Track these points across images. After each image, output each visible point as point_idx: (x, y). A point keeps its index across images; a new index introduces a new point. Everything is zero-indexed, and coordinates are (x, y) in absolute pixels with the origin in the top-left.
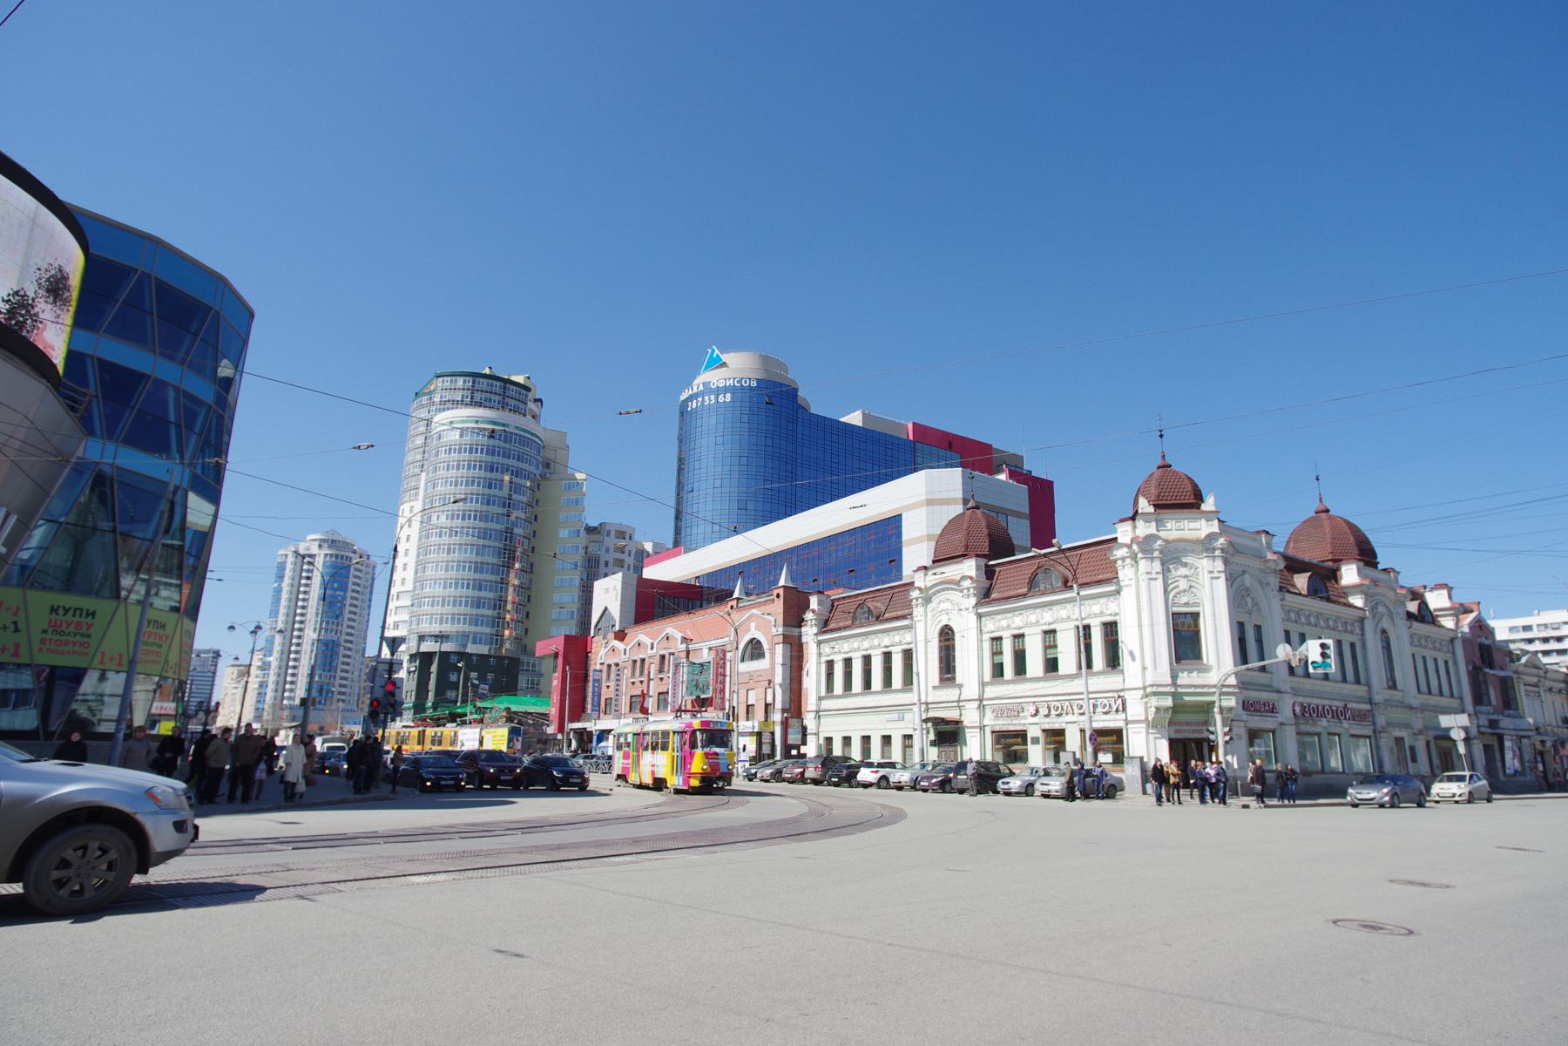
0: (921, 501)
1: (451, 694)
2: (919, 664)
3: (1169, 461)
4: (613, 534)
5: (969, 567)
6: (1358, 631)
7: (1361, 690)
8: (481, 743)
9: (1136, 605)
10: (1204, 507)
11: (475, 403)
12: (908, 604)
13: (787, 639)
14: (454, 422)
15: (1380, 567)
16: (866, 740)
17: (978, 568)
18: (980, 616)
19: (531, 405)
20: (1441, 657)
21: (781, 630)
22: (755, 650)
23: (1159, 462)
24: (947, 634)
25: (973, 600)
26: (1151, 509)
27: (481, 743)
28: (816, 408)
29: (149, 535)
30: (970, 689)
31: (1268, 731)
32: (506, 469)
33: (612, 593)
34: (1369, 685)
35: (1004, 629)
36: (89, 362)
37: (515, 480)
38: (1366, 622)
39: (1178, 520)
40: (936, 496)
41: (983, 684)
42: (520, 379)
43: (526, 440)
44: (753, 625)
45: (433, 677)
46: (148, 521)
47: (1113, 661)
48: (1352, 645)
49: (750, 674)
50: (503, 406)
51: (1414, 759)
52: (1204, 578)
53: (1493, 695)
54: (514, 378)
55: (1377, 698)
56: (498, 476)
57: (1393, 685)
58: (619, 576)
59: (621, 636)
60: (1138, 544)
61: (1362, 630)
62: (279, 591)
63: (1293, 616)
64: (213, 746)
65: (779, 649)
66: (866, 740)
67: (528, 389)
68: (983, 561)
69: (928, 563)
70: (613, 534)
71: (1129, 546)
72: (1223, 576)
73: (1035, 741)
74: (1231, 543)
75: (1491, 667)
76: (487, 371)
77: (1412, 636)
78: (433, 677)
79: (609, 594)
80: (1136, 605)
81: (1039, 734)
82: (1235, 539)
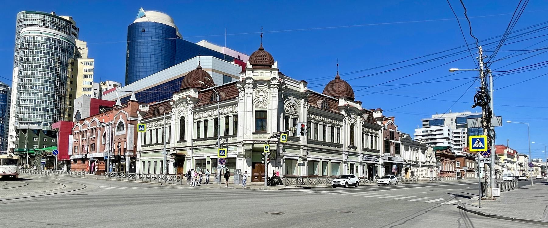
3: (263, 47)
8: (187, 158)
9: (245, 108)
10: (273, 67)
15: (355, 100)
23: (260, 47)
24: (183, 120)
26: (251, 67)
27: (187, 158)
28: (185, 38)
30: (189, 142)
35: (201, 118)
39: (260, 71)
42: (67, 18)
49: (120, 136)
51: (357, 171)
52: (270, 96)
53: (392, 149)
64: (259, 154)
72: (277, 96)
75: (393, 140)
76: (52, 13)
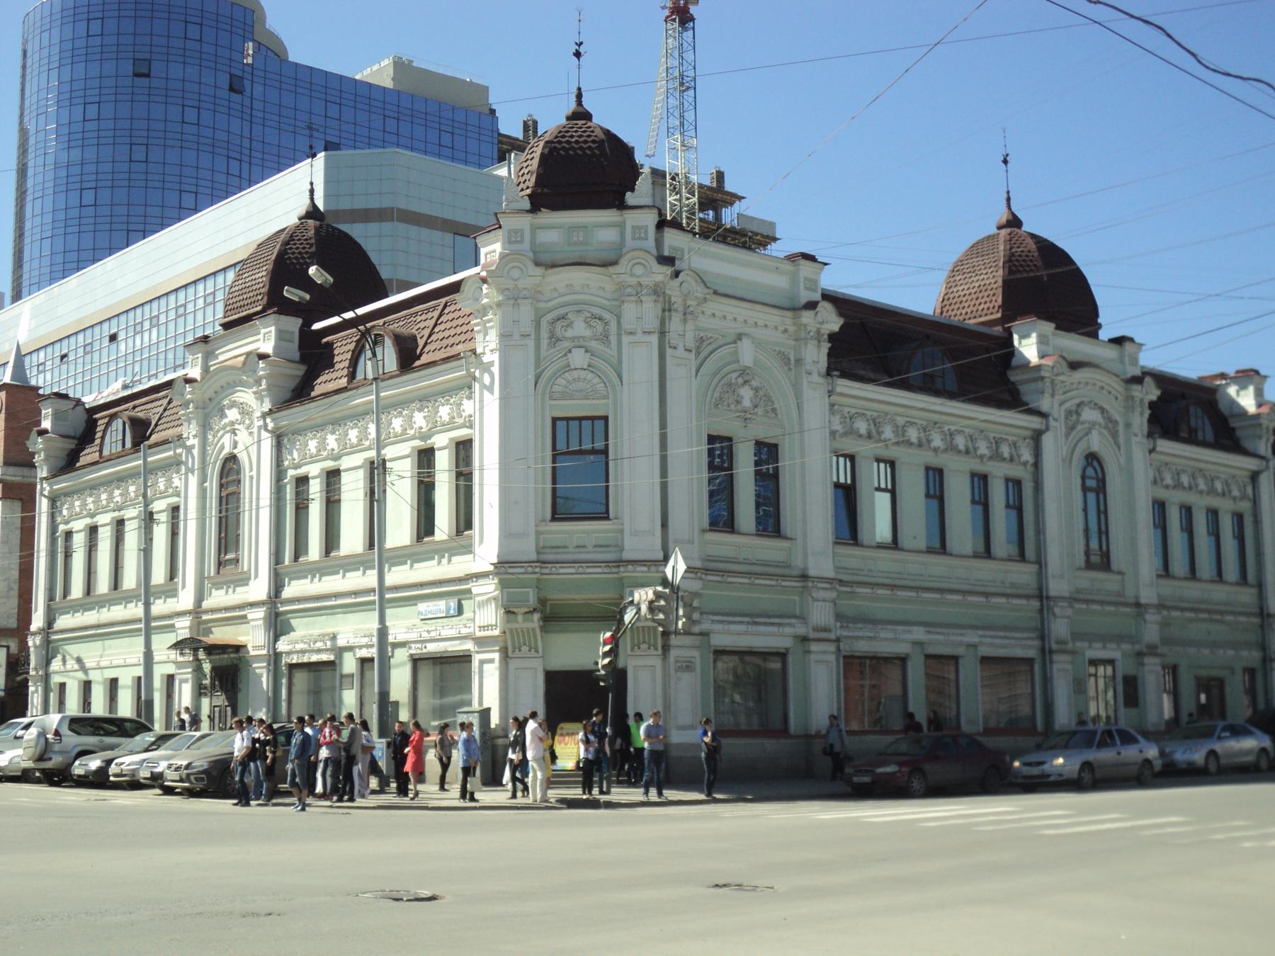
6: (1027, 456)
7: (1023, 574)
15: (1104, 334)
17: (281, 336)
20: (998, 472)
23: (1004, 217)
29: (258, 589)
31: (887, 660)
34: (1040, 562)
36: (1210, 436)
38: (1047, 441)
46: (93, 440)
48: (1239, 518)
55: (1056, 587)
57: (1100, 560)
61: (1037, 453)
62: (654, 681)
68: (294, 324)
69: (213, 329)
77: (832, 405)
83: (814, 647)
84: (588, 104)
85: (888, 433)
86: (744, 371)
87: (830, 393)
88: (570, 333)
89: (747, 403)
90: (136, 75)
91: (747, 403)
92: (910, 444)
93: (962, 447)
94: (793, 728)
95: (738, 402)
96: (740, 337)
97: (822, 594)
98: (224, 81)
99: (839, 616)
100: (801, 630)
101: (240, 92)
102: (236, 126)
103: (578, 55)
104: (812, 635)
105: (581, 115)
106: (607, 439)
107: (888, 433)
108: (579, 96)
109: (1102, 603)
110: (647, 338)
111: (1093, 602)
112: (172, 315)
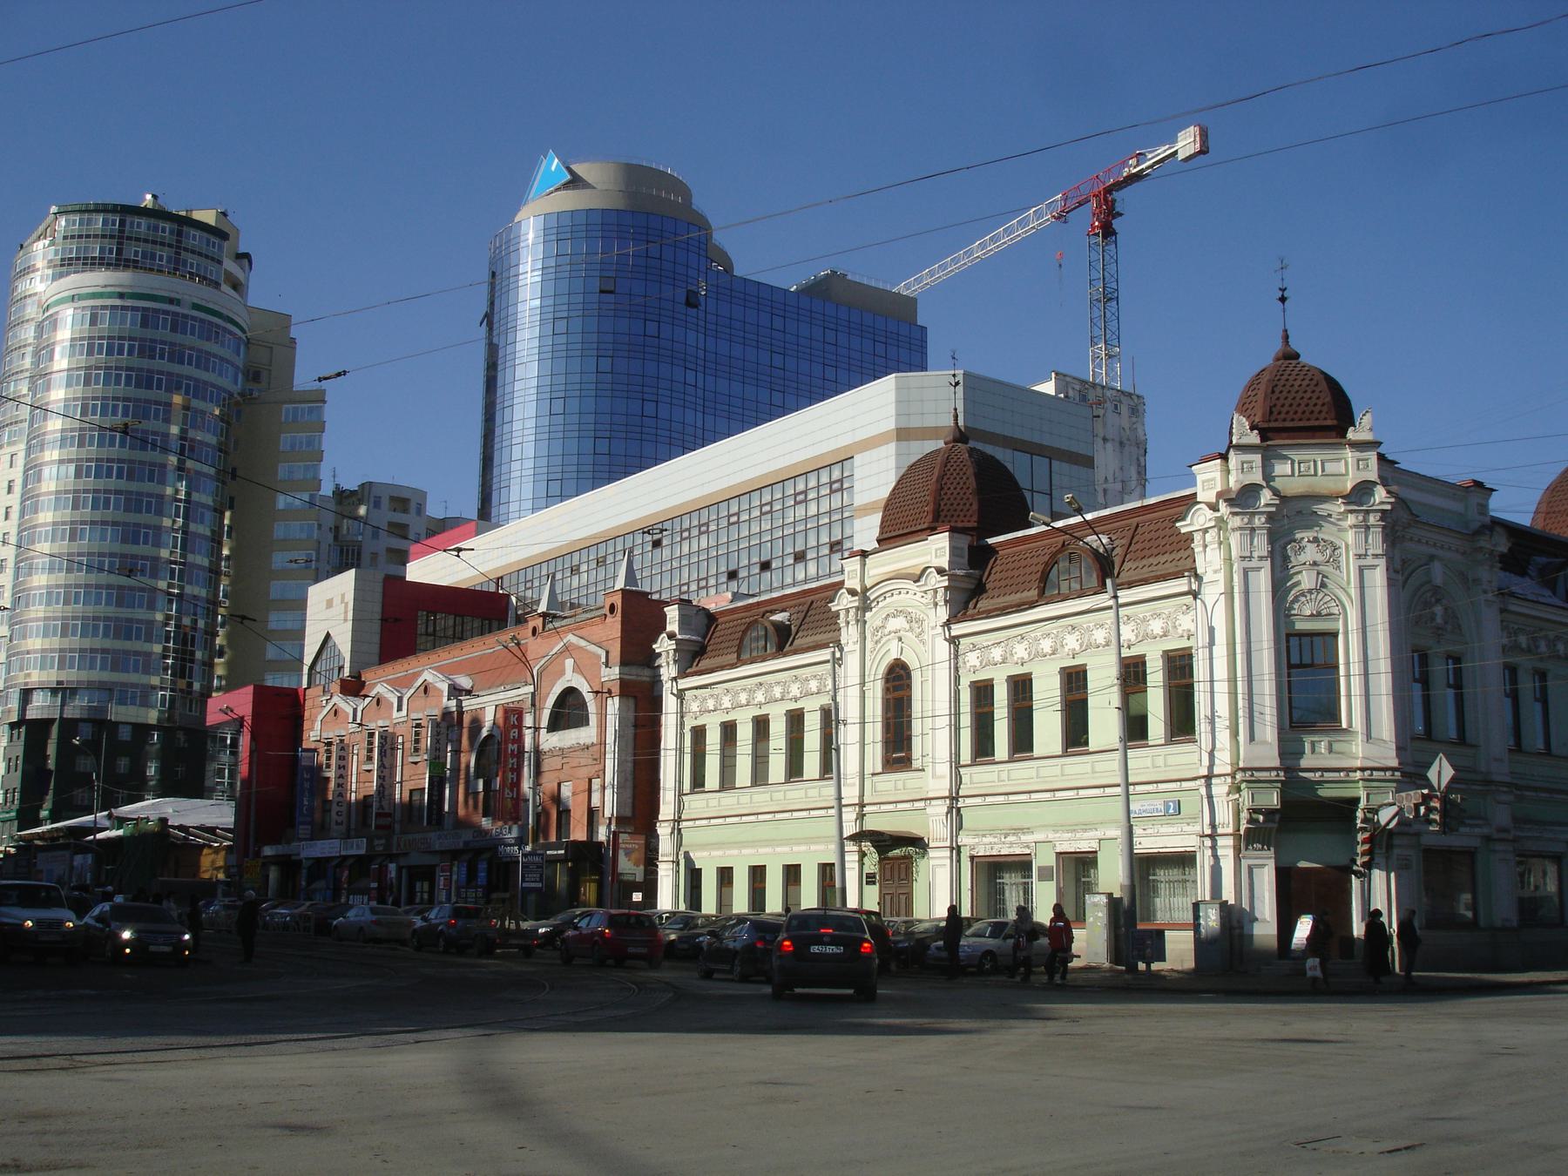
0: (863, 431)
1: (79, 794)
2: (848, 736)
4: (385, 503)
5: (936, 549)
9: (1208, 611)
10: (1351, 435)
11: (120, 262)
12: (831, 622)
13: (627, 689)
14: (60, 302)
16: (757, 874)
17: (954, 551)
18: (953, 641)
19: (229, 265)
21: (615, 672)
22: (569, 711)
25: (943, 613)
26: (1254, 438)
29: (942, 786)
32: (175, 384)
33: (338, 609)
37: (195, 403)
40: (915, 422)
41: (956, 765)
42: (208, 217)
43: (213, 323)
44: (569, 663)
45: (806, 990)
47: (1182, 724)
50: (176, 267)
51: (898, 745)
54: (198, 215)
56: (160, 395)
58: (351, 574)
59: (354, 687)
60: (1231, 502)
63: (1523, 640)
65: (613, 705)
66: (757, 874)
67: (223, 235)
68: (964, 542)
70: (385, 503)
71: (1214, 507)
72: (1382, 562)
73: (1045, 874)
74: (1400, 502)
78: (806, 990)
79: (331, 609)
80: (1208, 611)
81: (1051, 861)
82: (1410, 495)
83: (1499, 847)
84: (1295, 345)
85: (1543, 647)
86: (1436, 590)
87: (1502, 611)
88: (1302, 558)
89: (1439, 620)
90: (602, 292)
91: (1439, 620)
92: (1559, 657)
93: (1524, 646)
94: (1482, 923)
95: (1433, 619)
96: (1432, 558)
97: (1504, 798)
98: (681, 296)
99: (1515, 820)
100: (1486, 831)
101: (696, 306)
102: (692, 336)
103: (1283, 299)
104: (1496, 836)
105: (1290, 356)
106: (1288, 648)
107: (1543, 647)
108: (1286, 337)
109: (1535, 789)
110: (1376, 562)
111: (1528, 788)
112: (724, 523)
